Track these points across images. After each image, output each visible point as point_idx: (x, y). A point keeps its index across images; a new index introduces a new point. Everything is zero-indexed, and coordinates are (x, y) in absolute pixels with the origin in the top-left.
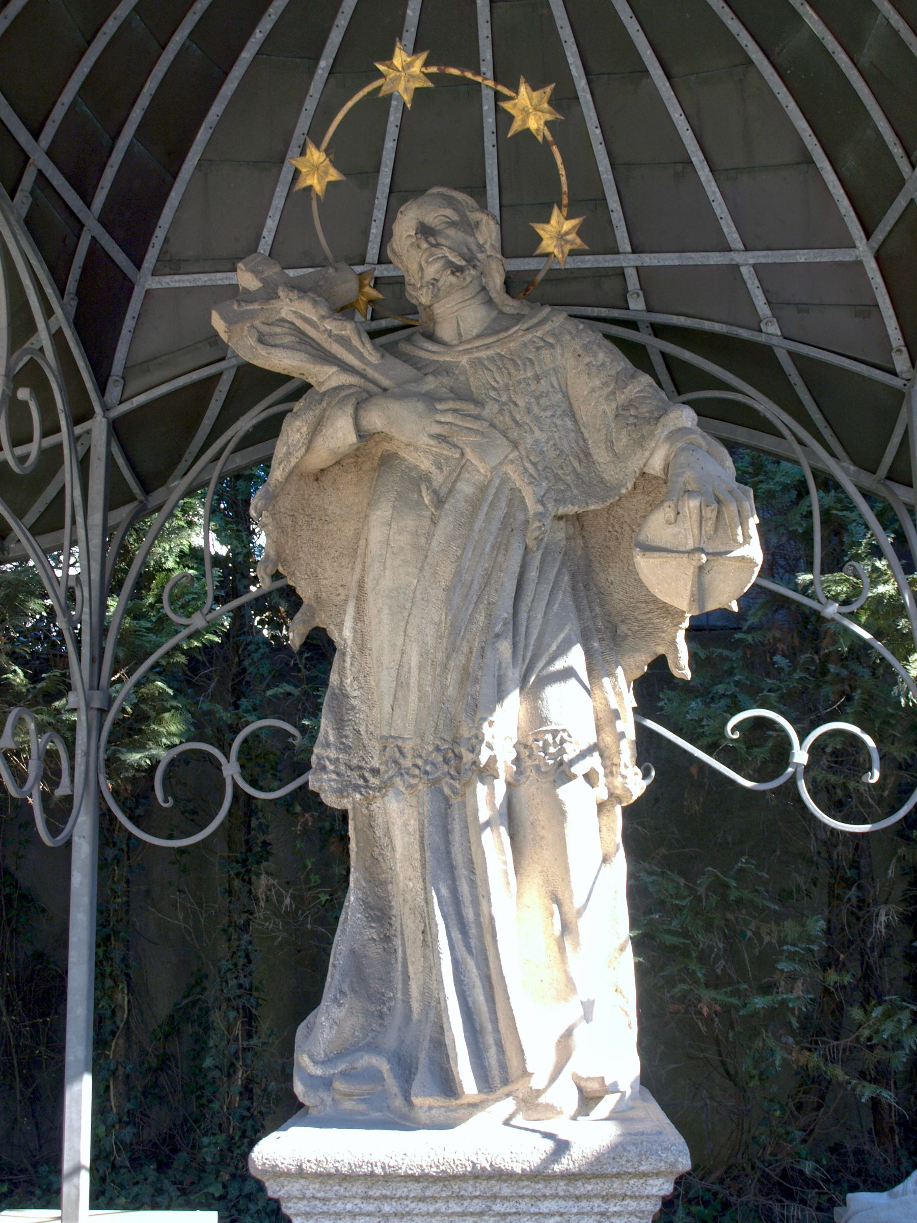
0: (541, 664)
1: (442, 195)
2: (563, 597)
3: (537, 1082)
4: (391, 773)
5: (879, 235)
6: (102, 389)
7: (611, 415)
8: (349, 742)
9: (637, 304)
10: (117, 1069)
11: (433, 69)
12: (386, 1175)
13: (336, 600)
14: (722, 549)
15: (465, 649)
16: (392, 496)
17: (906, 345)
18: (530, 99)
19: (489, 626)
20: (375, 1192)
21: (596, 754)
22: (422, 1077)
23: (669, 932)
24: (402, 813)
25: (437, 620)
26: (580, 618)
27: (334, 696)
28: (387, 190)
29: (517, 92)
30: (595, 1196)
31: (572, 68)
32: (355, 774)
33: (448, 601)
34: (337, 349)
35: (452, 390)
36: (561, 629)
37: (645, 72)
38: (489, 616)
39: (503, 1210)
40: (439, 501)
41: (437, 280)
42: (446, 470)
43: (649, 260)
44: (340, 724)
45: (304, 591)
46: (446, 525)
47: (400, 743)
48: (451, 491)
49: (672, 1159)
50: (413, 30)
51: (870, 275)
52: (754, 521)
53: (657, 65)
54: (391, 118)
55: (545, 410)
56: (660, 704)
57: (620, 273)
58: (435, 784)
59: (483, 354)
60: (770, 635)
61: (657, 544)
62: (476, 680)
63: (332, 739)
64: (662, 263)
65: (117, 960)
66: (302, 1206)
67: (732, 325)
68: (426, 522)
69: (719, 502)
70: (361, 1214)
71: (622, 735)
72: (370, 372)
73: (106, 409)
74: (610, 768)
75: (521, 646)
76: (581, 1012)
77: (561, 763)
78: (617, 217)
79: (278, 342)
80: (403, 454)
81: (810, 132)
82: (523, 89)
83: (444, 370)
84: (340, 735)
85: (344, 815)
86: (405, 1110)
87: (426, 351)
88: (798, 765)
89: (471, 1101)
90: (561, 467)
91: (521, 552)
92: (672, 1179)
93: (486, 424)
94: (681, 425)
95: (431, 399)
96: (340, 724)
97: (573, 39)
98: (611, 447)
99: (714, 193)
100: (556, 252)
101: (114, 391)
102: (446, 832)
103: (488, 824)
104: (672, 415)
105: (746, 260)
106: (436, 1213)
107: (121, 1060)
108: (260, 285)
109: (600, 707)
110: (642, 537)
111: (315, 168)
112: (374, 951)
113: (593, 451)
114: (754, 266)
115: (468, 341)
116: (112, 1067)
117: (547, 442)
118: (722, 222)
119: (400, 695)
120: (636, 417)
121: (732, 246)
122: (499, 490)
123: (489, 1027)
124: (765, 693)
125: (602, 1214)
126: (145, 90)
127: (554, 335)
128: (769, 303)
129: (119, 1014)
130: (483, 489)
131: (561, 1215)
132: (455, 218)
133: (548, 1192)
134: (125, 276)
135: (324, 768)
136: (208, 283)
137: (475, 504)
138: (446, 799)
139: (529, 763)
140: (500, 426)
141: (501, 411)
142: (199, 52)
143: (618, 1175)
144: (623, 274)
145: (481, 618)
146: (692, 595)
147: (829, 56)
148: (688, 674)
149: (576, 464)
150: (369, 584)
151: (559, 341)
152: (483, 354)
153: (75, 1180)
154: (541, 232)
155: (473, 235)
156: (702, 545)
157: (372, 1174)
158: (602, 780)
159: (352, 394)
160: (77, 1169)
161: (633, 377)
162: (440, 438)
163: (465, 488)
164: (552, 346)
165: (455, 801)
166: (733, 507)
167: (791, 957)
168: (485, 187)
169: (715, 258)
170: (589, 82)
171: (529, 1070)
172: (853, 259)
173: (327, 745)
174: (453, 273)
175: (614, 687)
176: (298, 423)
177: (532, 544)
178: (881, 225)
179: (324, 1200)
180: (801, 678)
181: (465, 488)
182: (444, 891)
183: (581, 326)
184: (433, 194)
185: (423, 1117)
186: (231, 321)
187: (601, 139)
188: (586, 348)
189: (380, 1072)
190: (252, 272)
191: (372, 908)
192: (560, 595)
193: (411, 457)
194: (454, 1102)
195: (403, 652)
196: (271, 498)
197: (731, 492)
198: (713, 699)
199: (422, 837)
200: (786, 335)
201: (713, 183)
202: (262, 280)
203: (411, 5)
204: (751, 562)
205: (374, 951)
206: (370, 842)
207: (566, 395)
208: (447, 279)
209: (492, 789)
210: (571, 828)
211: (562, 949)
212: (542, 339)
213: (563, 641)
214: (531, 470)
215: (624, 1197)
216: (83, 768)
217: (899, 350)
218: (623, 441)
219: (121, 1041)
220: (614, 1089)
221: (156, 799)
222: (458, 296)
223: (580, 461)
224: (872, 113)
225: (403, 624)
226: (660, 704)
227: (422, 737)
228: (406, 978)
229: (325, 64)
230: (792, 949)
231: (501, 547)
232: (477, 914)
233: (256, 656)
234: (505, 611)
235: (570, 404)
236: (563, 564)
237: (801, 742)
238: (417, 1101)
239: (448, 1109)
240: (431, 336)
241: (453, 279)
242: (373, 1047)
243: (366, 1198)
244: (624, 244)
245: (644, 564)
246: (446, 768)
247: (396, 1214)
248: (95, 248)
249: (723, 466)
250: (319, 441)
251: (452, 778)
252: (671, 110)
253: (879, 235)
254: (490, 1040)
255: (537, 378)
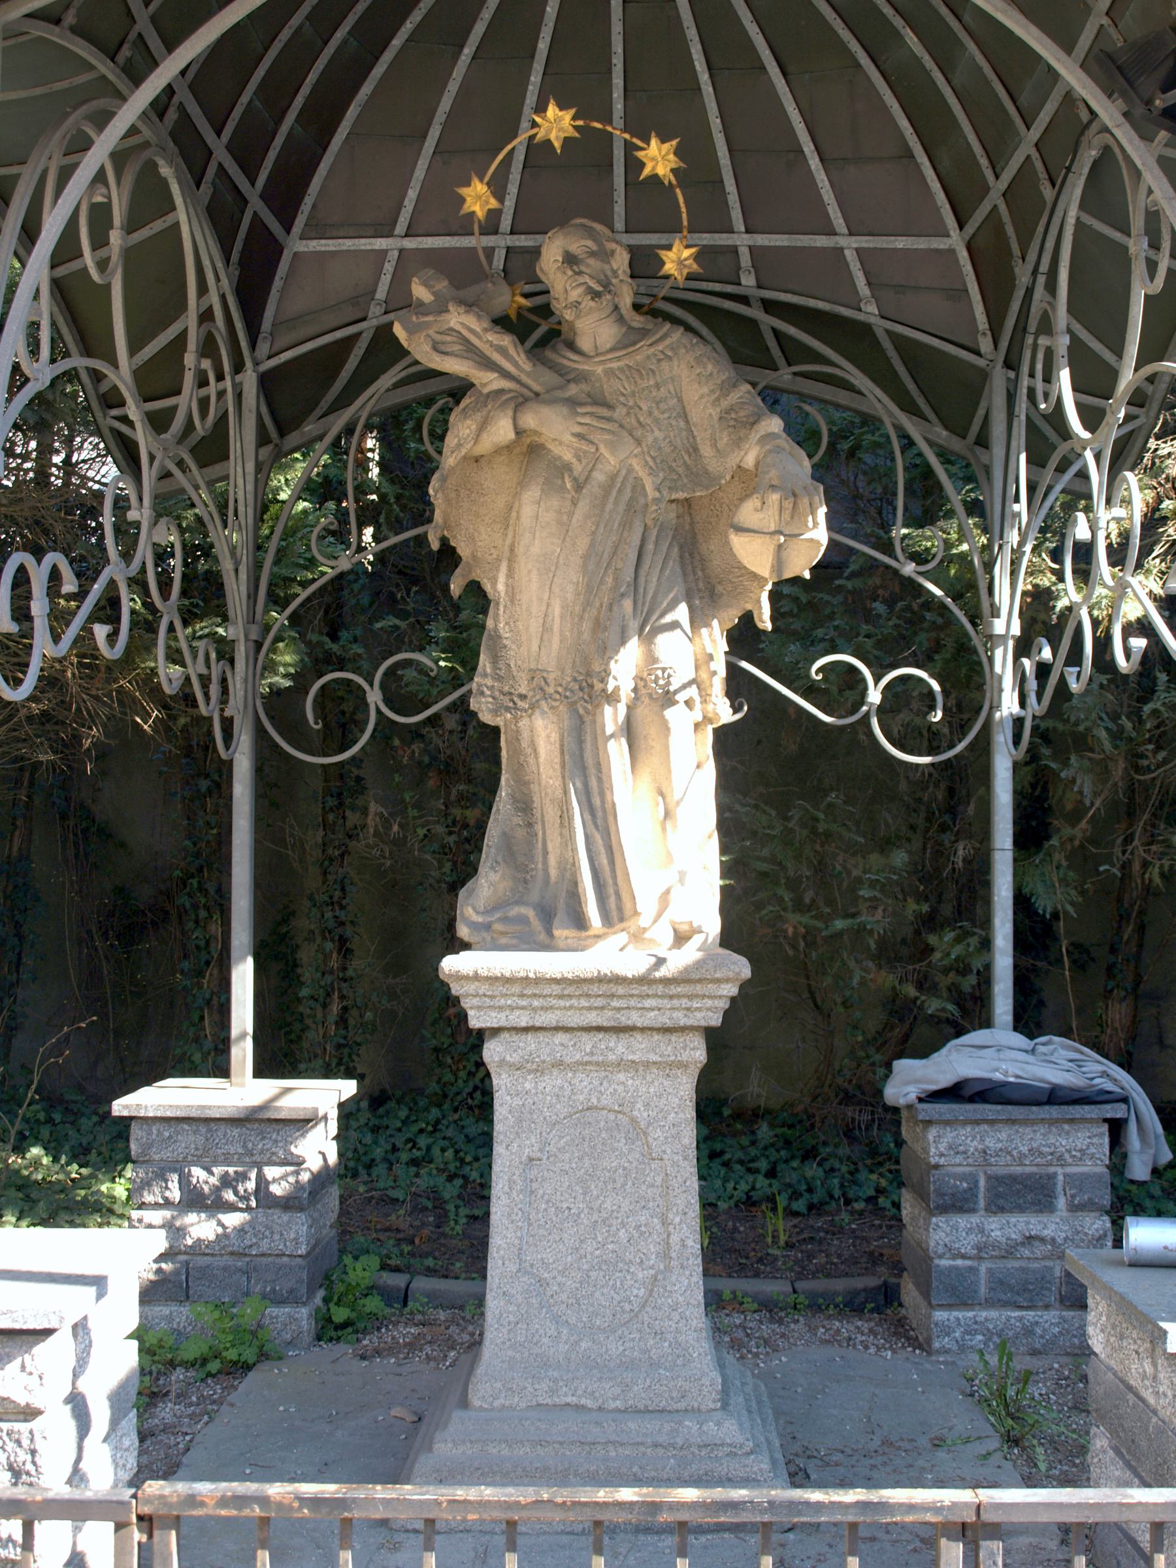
0: (654, 617)
1: (583, 226)
2: (673, 565)
3: (644, 921)
4: (538, 697)
5: (970, 229)
6: (253, 345)
7: (716, 418)
8: (502, 673)
9: (748, 280)
10: (211, 999)
11: (580, 123)
12: (537, 978)
13: (490, 558)
14: (796, 532)
15: (597, 604)
16: (541, 480)
17: (991, 329)
18: (660, 150)
19: (616, 587)
20: (528, 991)
21: (694, 687)
22: (561, 916)
23: (759, 859)
24: (546, 727)
25: (575, 580)
26: (686, 581)
27: (491, 637)
28: (521, 166)
29: (648, 145)
30: (683, 996)
31: (696, 63)
32: (507, 698)
33: (584, 567)
34: (496, 357)
35: (589, 395)
36: (670, 591)
37: (763, 68)
38: (616, 579)
39: (618, 1005)
40: (579, 487)
41: (579, 303)
42: (584, 462)
43: (762, 240)
44: (495, 659)
45: (463, 551)
46: (583, 507)
47: (545, 675)
48: (587, 479)
49: (737, 970)
50: (551, 25)
51: (962, 262)
52: (822, 511)
53: (774, 63)
54: (528, 101)
55: (663, 413)
56: (761, 646)
57: (734, 250)
58: (572, 706)
59: (614, 365)
60: (870, 582)
61: (747, 525)
62: (606, 629)
63: (489, 670)
64: (772, 244)
65: (212, 891)
66: (475, 1001)
67: (834, 303)
68: (568, 503)
69: (795, 495)
70: (517, 1008)
71: (715, 673)
72: (524, 378)
73: (256, 364)
74: (705, 697)
75: (640, 603)
76: (677, 877)
77: (668, 692)
78: (733, 198)
79: (449, 350)
80: (550, 446)
81: (911, 130)
82: (654, 142)
83: (582, 377)
84: (495, 668)
85: (496, 731)
86: (547, 941)
87: (570, 360)
88: (872, 704)
89: (597, 933)
90: (675, 460)
91: (642, 530)
92: (738, 984)
93: (617, 425)
94: (770, 431)
95: (573, 403)
96: (495, 659)
97: (697, 38)
98: (714, 444)
99: (822, 181)
100: (676, 274)
101: (263, 348)
102: (581, 742)
103: (612, 736)
104: (763, 423)
105: (850, 245)
106: (571, 1007)
107: (215, 990)
108: (433, 298)
109: (699, 651)
110: (736, 520)
111: (479, 197)
112: (520, 833)
113: (700, 447)
114: (857, 250)
115: (601, 354)
116: (207, 996)
117: (664, 439)
118: (830, 209)
119: (545, 637)
120: (735, 420)
121: (838, 230)
122: (625, 478)
123: (610, 881)
124: (860, 638)
125: (688, 1009)
126: (307, 81)
127: (672, 349)
128: (869, 284)
129: (213, 945)
130: (613, 477)
131: (659, 1009)
132: (595, 248)
133: (650, 992)
134: (276, 240)
135: (482, 693)
136: (352, 248)
137: (607, 489)
138: (581, 717)
139: (644, 691)
140: (628, 427)
141: (628, 414)
142: (355, 43)
143: (700, 981)
144: (737, 252)
145: (609, 580)
146: (773, 566)
147: (928, 74)
148: (769, 626)
149: (686, 458)
150: (520, 550)
151: (676, 354)
152: (614, 365)
153: (242, 1044)
154: (665, 258)
155: (609, 263)
156: (782, 529)
157: (527, 978)
158: (698, 706)
159: (511, 399)
160: (243, 1036)
161: (735, 386)
162: (579, 436)
163: (599, 477)
164: (670, 358)
165: (587, 719)
166: (806, 501)
167: (873, 884)
168: (612, 165)
169: (821, 241)
170: (711, 76)
171: (639, 910)
172: (946, 247)
173: (485, 675)
174: (592, 299)
175: (710, 635)
176: (468, 422)
177: (650, 523)
178: (971, 221)
179: (492, 997)
180: (896, 625)
181: (599, 477)
182: (579, 785)
183: (695, 341)
184: (576, 225)
185: (561, 944)
186: (411, 331)
187: (720, 127)
188: (698, 360)
189: (527, 918)
190: (426, 286)
191: (518, 801)
192: (671, 564)
193: (556, 450)
194: (584, 934)
195: (548, 605)
196: (444, 479)
197: (805, 488)
198: (812, 641)
199: (562, 746)
200: (884, 314)
201: (823, 172)
202: (433, 293)
203: (550, 3)
204: (818, 543)
205: (520, 833)
206: (516, 752)
207: (680, 400)
208: (587, 303)
209: (616, 710)
210: (673, 740)
211: (664, 829)
212: (662, 352)
213: (672, 599)
214: (651, 463)
215: (704, 996)
216: (242, 693)
217: (984, 334)
218: (724, 440)
219: (215, 972)
220: (699, 931)
221: (307, 721)
222: (595, 316)
223: (690, 455)
224: (963, 126)
225: (549, 583)
226: (761, 646)
227: (563, 671)
228: (546, 853)
229: (468, 51)
230: (873, 877)
231: (626, 524)
232: (603, 802)
233: (356, 587)
234: (628, 576)
235: (684, 408)
236: (674, 537)
237: (876, 684)
238: (557, 933)
239: (579, 939)
240: (571, 346)
241: (592, 304)
242: (519, 902)
243: (522, 996)
244: (739, 223)
245: (738, 542)
246: (581, 694)
247: (542, 1008)
248: (256, 217)
249: (801, 465)
250: (484, 436)
251: (586, 701)
252: (786, 104)
253: (970, 229)
254: (611, 891)
255: (657, 386)
